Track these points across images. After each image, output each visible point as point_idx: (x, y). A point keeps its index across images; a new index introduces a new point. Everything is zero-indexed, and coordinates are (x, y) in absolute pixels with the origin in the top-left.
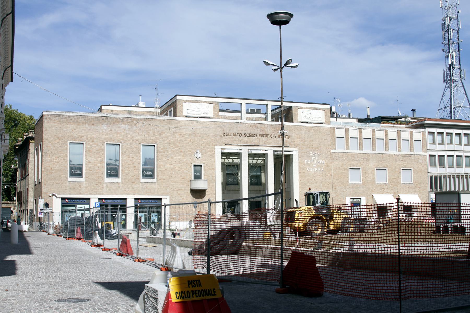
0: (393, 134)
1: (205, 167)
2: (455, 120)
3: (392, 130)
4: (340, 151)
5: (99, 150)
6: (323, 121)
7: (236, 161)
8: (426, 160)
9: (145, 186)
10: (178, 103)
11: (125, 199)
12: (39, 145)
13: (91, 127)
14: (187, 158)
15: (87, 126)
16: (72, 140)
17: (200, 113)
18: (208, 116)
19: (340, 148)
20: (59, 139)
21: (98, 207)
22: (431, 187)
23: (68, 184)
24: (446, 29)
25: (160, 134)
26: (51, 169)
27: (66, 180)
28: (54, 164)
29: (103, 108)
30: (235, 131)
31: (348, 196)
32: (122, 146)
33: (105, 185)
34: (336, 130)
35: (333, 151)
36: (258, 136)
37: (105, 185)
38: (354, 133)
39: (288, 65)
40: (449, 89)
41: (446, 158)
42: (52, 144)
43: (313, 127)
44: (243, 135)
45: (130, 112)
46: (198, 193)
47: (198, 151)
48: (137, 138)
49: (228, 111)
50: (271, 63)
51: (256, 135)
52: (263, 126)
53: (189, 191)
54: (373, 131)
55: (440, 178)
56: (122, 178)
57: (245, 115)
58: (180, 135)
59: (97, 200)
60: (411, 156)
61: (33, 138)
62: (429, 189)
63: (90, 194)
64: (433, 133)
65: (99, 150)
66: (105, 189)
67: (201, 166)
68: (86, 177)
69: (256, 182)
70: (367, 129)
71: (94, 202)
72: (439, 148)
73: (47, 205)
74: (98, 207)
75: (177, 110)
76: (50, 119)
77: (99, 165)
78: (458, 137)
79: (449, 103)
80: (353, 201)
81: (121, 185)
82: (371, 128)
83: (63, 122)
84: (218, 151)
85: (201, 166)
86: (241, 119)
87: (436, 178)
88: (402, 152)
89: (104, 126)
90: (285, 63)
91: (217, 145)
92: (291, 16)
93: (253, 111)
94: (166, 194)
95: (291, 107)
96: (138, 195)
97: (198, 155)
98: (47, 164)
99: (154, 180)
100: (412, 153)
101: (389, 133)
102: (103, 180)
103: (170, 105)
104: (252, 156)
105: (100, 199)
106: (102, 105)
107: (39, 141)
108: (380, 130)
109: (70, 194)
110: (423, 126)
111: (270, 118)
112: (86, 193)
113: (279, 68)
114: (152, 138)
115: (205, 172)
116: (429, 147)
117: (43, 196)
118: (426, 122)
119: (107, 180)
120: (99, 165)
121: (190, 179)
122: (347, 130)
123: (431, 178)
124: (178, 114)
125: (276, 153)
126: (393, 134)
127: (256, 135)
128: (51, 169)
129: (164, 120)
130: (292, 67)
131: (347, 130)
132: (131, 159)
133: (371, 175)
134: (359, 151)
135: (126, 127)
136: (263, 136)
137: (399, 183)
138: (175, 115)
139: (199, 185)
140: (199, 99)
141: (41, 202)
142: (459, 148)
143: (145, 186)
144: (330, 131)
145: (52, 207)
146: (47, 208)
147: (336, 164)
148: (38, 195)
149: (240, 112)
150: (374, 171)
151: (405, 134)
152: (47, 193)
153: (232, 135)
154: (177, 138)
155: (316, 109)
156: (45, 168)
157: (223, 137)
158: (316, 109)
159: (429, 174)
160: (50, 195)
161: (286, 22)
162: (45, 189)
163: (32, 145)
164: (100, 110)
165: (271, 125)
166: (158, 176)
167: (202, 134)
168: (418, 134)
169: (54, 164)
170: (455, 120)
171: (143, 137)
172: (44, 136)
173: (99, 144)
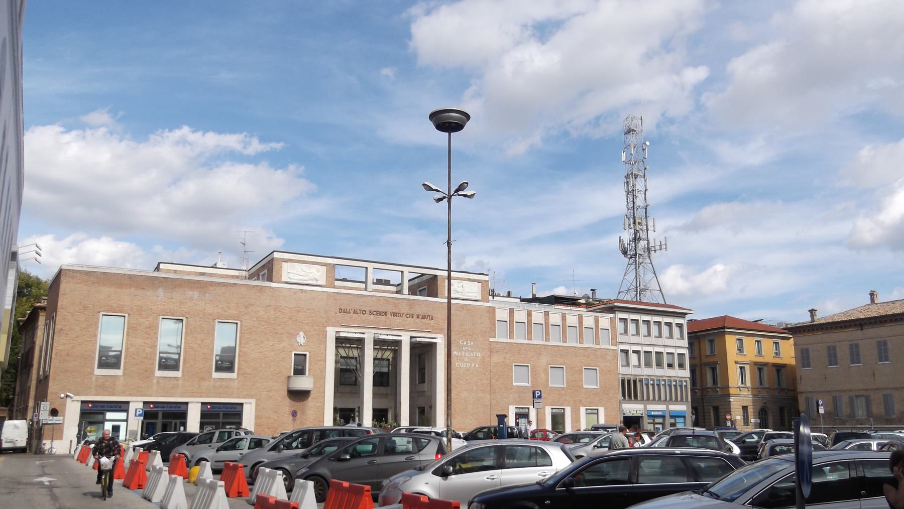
0: (572, 320)
1: (310, 357)
2: (642, 303)
3: (572, 315)
4: (501, 340)
5: (149, 327)
6: (479, 298)
7: (355, 353)
8: (616, 356)
9: (218, 384)
10: (275, 263)
11: (187, 403)
12: (51, 318)
13: (139, 292)
14: (284, 344)
15: (133, 290)
16: (107, 311)
17: (306, 278)
18: (319, 283)
19: (500, 337)
20: (85, 308)
21: (140, 415)
22: (624, 395)
23: (94, 379)
24: (630, 189)
25: (246, 307)
26: (68, 355)
27: (92, 373)
28: (73, 347)
29: (162, 266)
30: (356, 306)
31: (512, 404)
32: (187, 322)
33: (155, 381)
34: (497, 311)
35: (491, 339)
36: (389, 315)
37: (155, 381)
38: (520, 316)
39: (460, 193)
40: (633, 266)
41: (665, 355)
42: (73, 315)
43: (465, 305)
44: (368, 312)
45: (203, 274)
46: (299, 395)
47: (302, 334)
48: (210, 312)
49: (345, 280)
50: (434, 187)
51: (385, 313)
52: (396, 302)
53: (286, 393)
54: (547, 314)
55: (635, 382)
56: (183, 372)
57: (371, 286)
58: (276, 309)
59: (141, 406)
60: (596, 350)
61: (43, 308)
62: (621, 398)
63: (130, 395)
64: (624, 320)
65: (149, 327)
66: (155, 387)
67: (305, 355)
68: (125, 369)
69: (385, 380)
70: (538, 312)
71: (136, 405)
72: (634, 341)
73: (54, 412)
74: (140, 415)
75: (274, 273)
76: (73, 277)
77: (148, 350)
78: (667, 328)
79: (634, 284)
80: (518, 410)
81: (181, 382)
82: (543, 309)
83: (93, 283)
84: (331, 333)
85: (305, 355)
86: (366, 289)
87: (629, 381)
88: (585, 345)
89: (161, 292)
90: (456, 187)
91: (329, 326)
92: (468, 117)
93: (379, 282)
94: (251, 397)
95: (436, 276)
96: (208, 397)
97: (301, 339)
98: (61, 348)
99: (234, 375)
100: (598, 346)
101: (568, 317)
102: (153, 373)
103: (264, 266)
104: (379, 344)
105: (145, 403)
106: (159, 263)
107: (52, 310)
108: (556, 313)
109: (97, 395)
110: (611, 309)
111: (406, 291)
112: (123, 393)
113: (444, 198)
114: (234, 312)
115: (310, 365)
116: (620, 338)
117: (49, 398)
118: (616, 304)
119: (159, 373)
120: (148, 350)
121: (288, 374)
122: (511, 312)
123: (623, 381)
124: (274, 279)
125: (413, 340)
126: (572, 320)
127: (385, 313)
128: (68, 355)
129: (254, 287)
130: (465, 196)
131: (511, 312)
132: (199, 342)
133: (542, 375)
134: (526, 342)
135: (195, 294)
136: (395, 314)
137: (581, 387)
138: (270, 279)
139: (302, 383)
140: (306, 258)
141: (45, 407)
142: (659, 341)
143: (218, 384)
144: (489, 312)
145: (64, 416)
146: (55, 418)
147: (496, 358)
148: (42, 395)
149: (365, 283)
150: (581, 371)
151: (589, 319)
152: (56, 394)
153: (352, 312)
154: (272, 313)
155: (469, 280)
156: (56, 354)
157: (338, 314)
158: (469, 280)
159: (620, 376)
160: (62, 396)
161: (458, 127)
162: (52, 387)
163: (42, 319)
164: (157, 268)
165: (408, 300)
166: (239, 368)
167: (308, 309)
168: (605, 320)
169: (73, 347)
170: (642, 303)
171: (220, 311)
172: (59, 303)
173: (151, 319)
